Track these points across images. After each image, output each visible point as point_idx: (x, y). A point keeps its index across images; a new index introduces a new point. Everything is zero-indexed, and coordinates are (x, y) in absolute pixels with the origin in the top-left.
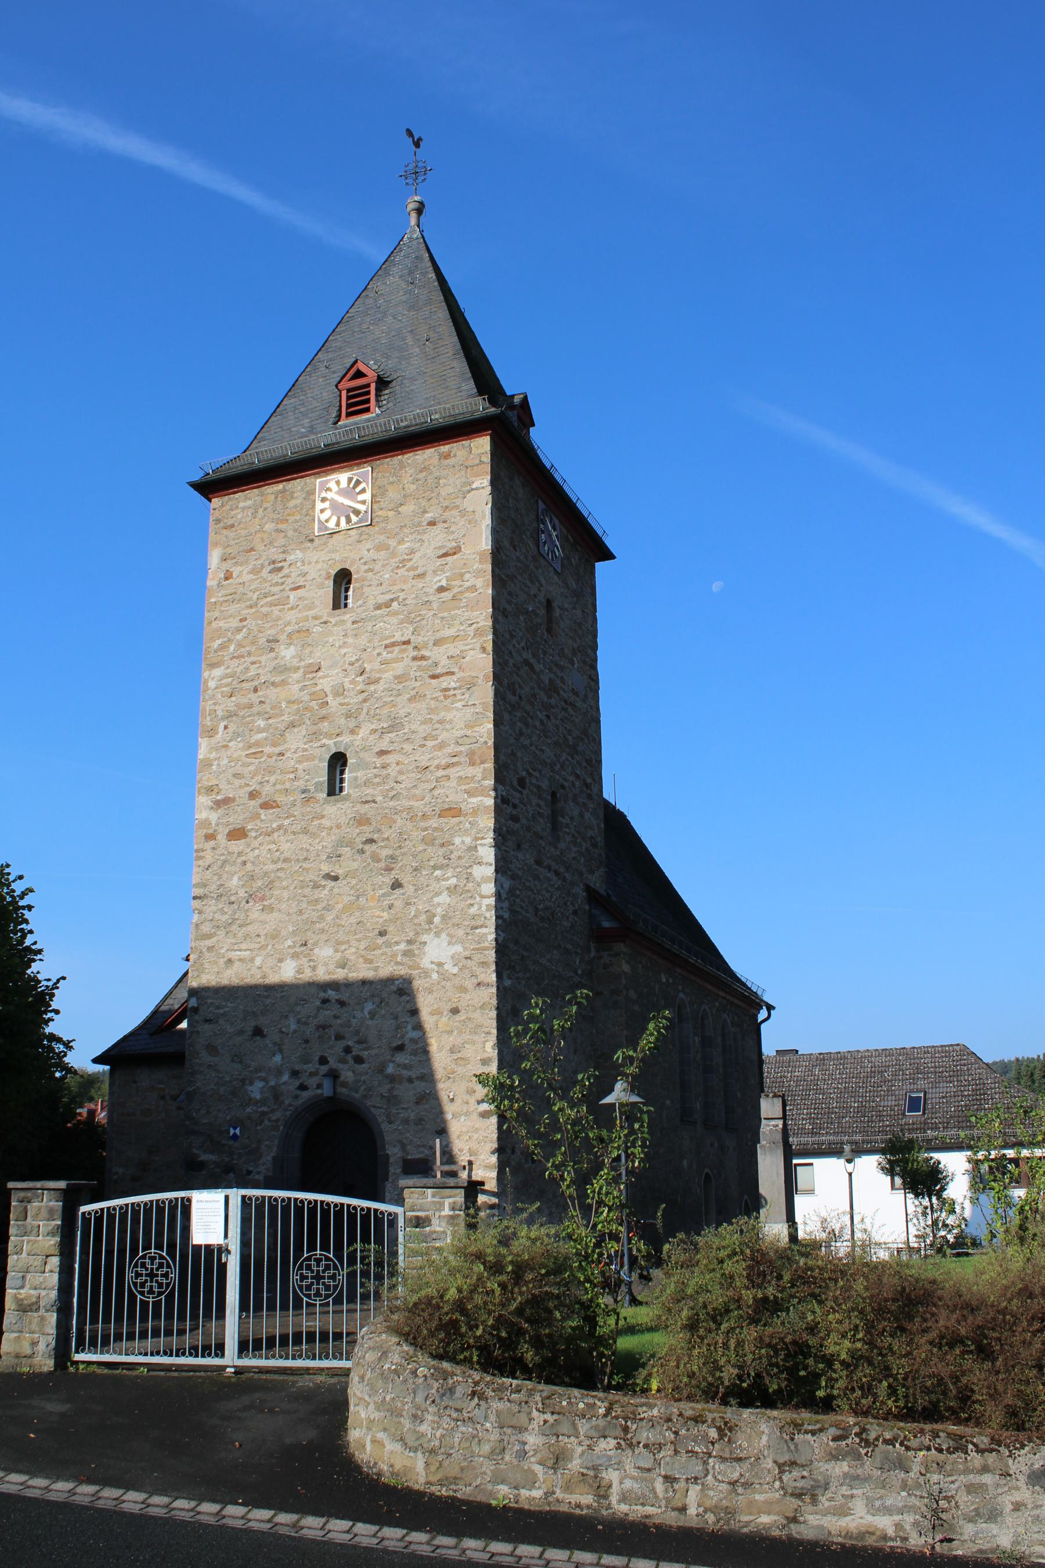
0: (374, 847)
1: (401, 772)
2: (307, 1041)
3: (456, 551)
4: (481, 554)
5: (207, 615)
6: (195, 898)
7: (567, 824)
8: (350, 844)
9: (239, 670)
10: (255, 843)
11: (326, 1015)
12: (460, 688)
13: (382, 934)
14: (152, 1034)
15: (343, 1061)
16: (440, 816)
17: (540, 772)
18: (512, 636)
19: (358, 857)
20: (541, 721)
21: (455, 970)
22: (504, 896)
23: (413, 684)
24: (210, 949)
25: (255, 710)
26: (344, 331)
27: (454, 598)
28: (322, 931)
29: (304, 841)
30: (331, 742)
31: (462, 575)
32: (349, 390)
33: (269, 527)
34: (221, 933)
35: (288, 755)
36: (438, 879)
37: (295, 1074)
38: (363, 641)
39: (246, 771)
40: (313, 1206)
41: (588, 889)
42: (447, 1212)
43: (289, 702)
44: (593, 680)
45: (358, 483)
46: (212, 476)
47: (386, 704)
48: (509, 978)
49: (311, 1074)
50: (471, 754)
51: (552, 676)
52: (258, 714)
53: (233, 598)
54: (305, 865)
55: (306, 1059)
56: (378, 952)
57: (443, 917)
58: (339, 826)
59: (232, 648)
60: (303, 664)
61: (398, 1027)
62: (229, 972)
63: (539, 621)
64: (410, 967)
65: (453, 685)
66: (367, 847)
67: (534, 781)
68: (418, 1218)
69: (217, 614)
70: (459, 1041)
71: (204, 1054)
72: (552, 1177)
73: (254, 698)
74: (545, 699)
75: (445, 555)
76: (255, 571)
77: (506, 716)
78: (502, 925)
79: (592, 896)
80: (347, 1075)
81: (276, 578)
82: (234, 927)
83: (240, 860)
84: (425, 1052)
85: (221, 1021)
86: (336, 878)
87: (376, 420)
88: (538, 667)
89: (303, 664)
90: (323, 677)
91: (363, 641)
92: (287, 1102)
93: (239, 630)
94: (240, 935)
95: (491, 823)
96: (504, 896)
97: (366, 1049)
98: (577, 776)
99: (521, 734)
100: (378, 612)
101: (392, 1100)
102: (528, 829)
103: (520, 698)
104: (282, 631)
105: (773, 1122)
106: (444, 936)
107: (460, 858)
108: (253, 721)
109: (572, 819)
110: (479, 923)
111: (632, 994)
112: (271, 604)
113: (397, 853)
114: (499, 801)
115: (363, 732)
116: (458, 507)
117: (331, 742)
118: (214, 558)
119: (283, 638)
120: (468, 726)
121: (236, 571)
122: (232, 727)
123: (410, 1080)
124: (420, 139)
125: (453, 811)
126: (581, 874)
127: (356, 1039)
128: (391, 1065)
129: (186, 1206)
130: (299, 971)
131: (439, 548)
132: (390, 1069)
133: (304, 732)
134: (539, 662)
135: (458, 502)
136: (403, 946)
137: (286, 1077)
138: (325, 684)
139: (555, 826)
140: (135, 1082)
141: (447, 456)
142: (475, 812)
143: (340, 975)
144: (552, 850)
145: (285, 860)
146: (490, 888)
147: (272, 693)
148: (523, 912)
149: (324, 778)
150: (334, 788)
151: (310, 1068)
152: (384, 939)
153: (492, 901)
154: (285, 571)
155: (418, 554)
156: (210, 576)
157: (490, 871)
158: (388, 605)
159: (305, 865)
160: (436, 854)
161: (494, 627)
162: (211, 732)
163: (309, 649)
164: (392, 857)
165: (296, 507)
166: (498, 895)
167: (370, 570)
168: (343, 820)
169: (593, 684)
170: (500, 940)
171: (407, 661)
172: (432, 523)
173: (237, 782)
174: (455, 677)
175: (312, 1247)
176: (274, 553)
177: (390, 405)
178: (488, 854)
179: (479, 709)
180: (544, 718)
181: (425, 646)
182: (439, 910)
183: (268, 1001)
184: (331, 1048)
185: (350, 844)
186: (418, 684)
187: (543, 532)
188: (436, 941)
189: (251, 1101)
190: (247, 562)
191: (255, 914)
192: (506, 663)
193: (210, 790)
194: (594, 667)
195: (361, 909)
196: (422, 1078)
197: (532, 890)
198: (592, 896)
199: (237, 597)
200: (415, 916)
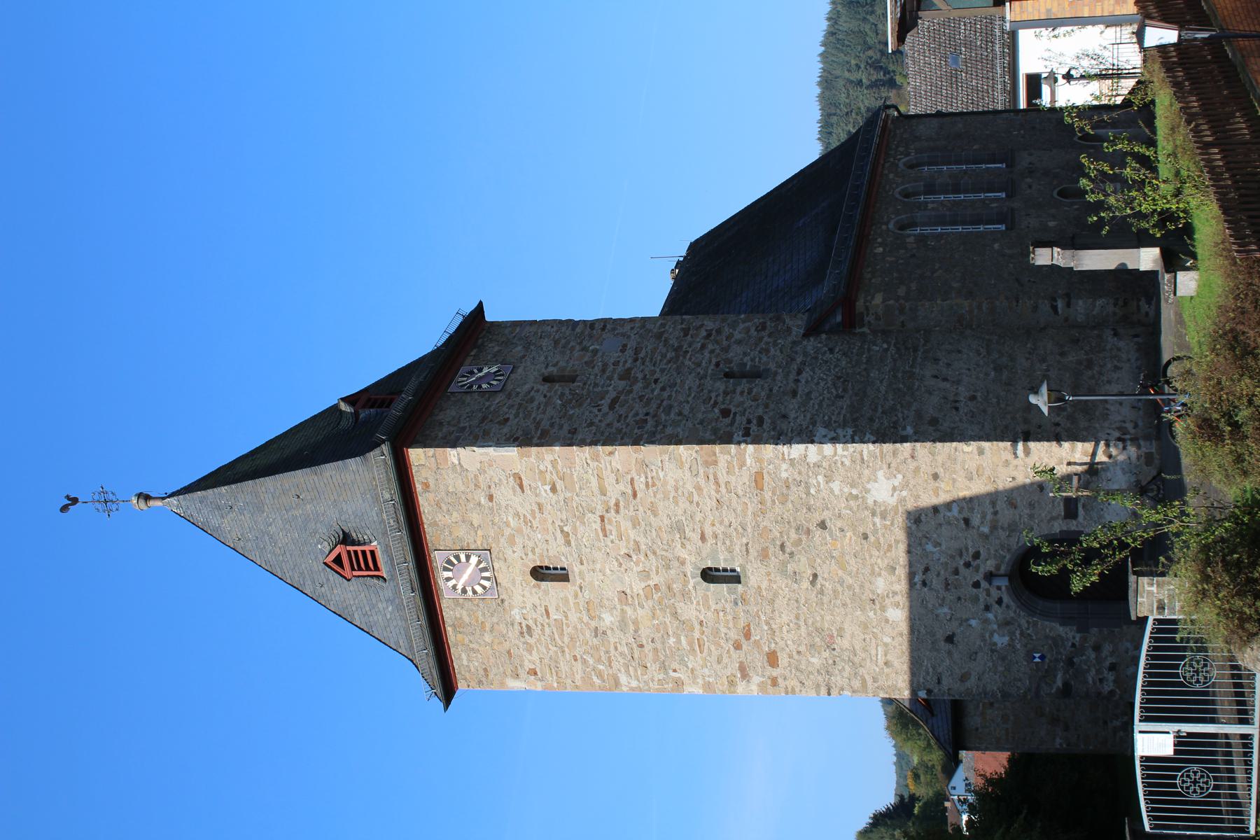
0: (788, 544)
1: (721, 523)
2: (959, 599)
3: (518, 478)
4: (521, 456)
5: (569, 690)
6: (829, 694)
7: (752, 360)
8: (784, 564)
9: (622, 661)
10: (782, 644)
11: (936, 583)
12: (646, 474)
13: (865, 537)
14: (933, 715)
15: (977, 569)
16: (762, 490)
17: (710, 392)
18: (591, 424)
19: (796, 558)
20: (663, 389)
21: (900, 477)
22: (832, 434)
23: (640, 514)
24: (875, 680)
25: (659, 646)
26: (281, 569)
27: (562, 479)
28: (862, 586)
29: (780, 602)
30: (692, 582)
31: (541, 472)
32: (353, 569)
33: (488, 638)
34: (861, 671)
35: (702, 618)
36: (818, 491)
37: (987, 608)
38: (599, 555)
39: (715, 653)
40: (1147, 675)
41: (806, 335)
42: (1154, 589)
43: (654, 618)
44: (605, 326)
45: (449, 562)
46: (439, 690)
47: (658, 535)
48: (904, 428)
49: (988, 595)
50: (706, 464)
51: (616, 376)
52: (663, 643)
53: (555, 667)
54: (803, 601)
55: (976, 599)
56: (882, 540)
57: (852, 486)
58: (768, 574)
59: (601, 667)
60: (618, 607)
61: (949, 523)
62: (896, 663)
63: (567, 392)
64: (896, 514)
65: (643, 479)
66: (788, 550)
67: (720, 399)
68: (1158, 608)
69: (569, 681)
70: (962, 473)
71: (968, 684)
72: (1143, 543)
73: (648, 647)
74: (640, 385)
75: (521, 486)
76: (529, 649)
77: (669, 430)
78: (858, 436)
79: (812, 330)
80: (990, 565)
81: (537, 631)
82: (856, 660)
83: (796, 657)
84: (970, 501)
85: (940, 670)
86: (815, 576)
87: (388, 545)
88: (613, 395)
89: (618, 607)
90: (631, 588)
91: (599, 555)
92: (1012, 615)
93: (585, 662)
94: (863, 655)
95: (770, 447)
96: (832, 434)
97: (967, 549)
98: (703, 347)
99: (680, 414)
100: (573, 543)
101: (1013, 528)
102: (766, 406)
103: (647, 414)
104: (587, 624)
105: (1055, 255)
106: (869, 486)
107: (800, 473)
108: (670, 648)
109: (745, 354)
110: (858, 456)
111: (902, 291)
112: (562, 634)
113: (793, 524)
114: (749, 439)
115: (683, 554)
116: (476, 476)
117: (692, 582)
118: (514, 684)
119: (593, 624)
120: (681, 466)
121: (528, 666)
122: (675, 665)
123: (996, 513)
124: (68, 497)
125: (758, 479)
126: (794, 343)
127: (958, 558)
128: (982, 529)
129: (1146, 759)
130: (897, 605)
131: (514, 491)
132: (986, 530)
133: (682, 604)
134: (607, 392)
135: (471, 476)
136: (877, 520)
137: (990, 616)
138: (638, 587)
139: (756, 374)
140: (977, 729)
141: (426, 485)
142: (759, 460)
143: (902, 572)
144: (779, 378)
145: (797, 618)
146: (828, 448)
147: (645, 633)
148: (844, 412)
149: (724, 587)
150: (733, 578)
151: (982, 596)
152: (870, 535)
153: (839, 446)
154: (531, 623)
155: (520, 509)
156: (533, 688)
157: (812, 448)
158: (566, 535)
159: (803, 601)
160: (796, 493)
161: (590, 444)
162: (679, 683)
163: (605, 601)
164: (798, 529)
165: (469, 616)
166: (834, 440)
167: (533, 551)
168: (763, 570)
169: (609, 327)
170: (873, 438)
171: (619, 518)
172: (491, 498)
173: (725, 660)
174: (636, 478)
175: (1177, 676)
176: (513, 634)
177: (368, 532)
178: (797, 450)
179: (666, 457)
180: (660, 385)
181: (606, 503)
182: (846, 490)
183: (923, 631)
184: (965, 578)
185: (784, 564)
186: (641, 509)
187: (480, 387)
188: (873, 492)
189: (1011, 645)
190: (521, 657)
191: (844, 643)
192: (619, 431)
193: (732, 683)
194: (591, 324)
195: (843, 554)
196: (993, 504)
197: (821, 401)
198: (812, 330)
199: (553, 665)
200: (851, 510)
